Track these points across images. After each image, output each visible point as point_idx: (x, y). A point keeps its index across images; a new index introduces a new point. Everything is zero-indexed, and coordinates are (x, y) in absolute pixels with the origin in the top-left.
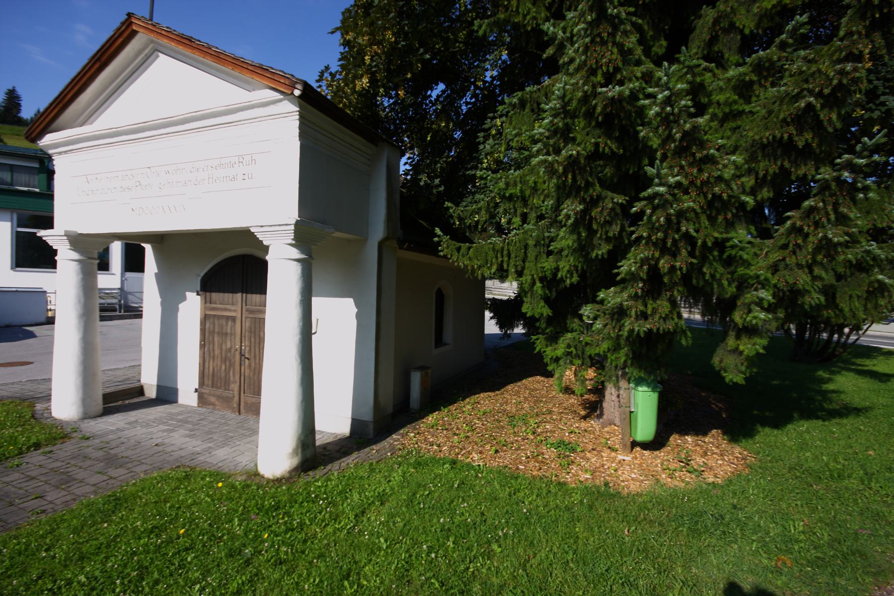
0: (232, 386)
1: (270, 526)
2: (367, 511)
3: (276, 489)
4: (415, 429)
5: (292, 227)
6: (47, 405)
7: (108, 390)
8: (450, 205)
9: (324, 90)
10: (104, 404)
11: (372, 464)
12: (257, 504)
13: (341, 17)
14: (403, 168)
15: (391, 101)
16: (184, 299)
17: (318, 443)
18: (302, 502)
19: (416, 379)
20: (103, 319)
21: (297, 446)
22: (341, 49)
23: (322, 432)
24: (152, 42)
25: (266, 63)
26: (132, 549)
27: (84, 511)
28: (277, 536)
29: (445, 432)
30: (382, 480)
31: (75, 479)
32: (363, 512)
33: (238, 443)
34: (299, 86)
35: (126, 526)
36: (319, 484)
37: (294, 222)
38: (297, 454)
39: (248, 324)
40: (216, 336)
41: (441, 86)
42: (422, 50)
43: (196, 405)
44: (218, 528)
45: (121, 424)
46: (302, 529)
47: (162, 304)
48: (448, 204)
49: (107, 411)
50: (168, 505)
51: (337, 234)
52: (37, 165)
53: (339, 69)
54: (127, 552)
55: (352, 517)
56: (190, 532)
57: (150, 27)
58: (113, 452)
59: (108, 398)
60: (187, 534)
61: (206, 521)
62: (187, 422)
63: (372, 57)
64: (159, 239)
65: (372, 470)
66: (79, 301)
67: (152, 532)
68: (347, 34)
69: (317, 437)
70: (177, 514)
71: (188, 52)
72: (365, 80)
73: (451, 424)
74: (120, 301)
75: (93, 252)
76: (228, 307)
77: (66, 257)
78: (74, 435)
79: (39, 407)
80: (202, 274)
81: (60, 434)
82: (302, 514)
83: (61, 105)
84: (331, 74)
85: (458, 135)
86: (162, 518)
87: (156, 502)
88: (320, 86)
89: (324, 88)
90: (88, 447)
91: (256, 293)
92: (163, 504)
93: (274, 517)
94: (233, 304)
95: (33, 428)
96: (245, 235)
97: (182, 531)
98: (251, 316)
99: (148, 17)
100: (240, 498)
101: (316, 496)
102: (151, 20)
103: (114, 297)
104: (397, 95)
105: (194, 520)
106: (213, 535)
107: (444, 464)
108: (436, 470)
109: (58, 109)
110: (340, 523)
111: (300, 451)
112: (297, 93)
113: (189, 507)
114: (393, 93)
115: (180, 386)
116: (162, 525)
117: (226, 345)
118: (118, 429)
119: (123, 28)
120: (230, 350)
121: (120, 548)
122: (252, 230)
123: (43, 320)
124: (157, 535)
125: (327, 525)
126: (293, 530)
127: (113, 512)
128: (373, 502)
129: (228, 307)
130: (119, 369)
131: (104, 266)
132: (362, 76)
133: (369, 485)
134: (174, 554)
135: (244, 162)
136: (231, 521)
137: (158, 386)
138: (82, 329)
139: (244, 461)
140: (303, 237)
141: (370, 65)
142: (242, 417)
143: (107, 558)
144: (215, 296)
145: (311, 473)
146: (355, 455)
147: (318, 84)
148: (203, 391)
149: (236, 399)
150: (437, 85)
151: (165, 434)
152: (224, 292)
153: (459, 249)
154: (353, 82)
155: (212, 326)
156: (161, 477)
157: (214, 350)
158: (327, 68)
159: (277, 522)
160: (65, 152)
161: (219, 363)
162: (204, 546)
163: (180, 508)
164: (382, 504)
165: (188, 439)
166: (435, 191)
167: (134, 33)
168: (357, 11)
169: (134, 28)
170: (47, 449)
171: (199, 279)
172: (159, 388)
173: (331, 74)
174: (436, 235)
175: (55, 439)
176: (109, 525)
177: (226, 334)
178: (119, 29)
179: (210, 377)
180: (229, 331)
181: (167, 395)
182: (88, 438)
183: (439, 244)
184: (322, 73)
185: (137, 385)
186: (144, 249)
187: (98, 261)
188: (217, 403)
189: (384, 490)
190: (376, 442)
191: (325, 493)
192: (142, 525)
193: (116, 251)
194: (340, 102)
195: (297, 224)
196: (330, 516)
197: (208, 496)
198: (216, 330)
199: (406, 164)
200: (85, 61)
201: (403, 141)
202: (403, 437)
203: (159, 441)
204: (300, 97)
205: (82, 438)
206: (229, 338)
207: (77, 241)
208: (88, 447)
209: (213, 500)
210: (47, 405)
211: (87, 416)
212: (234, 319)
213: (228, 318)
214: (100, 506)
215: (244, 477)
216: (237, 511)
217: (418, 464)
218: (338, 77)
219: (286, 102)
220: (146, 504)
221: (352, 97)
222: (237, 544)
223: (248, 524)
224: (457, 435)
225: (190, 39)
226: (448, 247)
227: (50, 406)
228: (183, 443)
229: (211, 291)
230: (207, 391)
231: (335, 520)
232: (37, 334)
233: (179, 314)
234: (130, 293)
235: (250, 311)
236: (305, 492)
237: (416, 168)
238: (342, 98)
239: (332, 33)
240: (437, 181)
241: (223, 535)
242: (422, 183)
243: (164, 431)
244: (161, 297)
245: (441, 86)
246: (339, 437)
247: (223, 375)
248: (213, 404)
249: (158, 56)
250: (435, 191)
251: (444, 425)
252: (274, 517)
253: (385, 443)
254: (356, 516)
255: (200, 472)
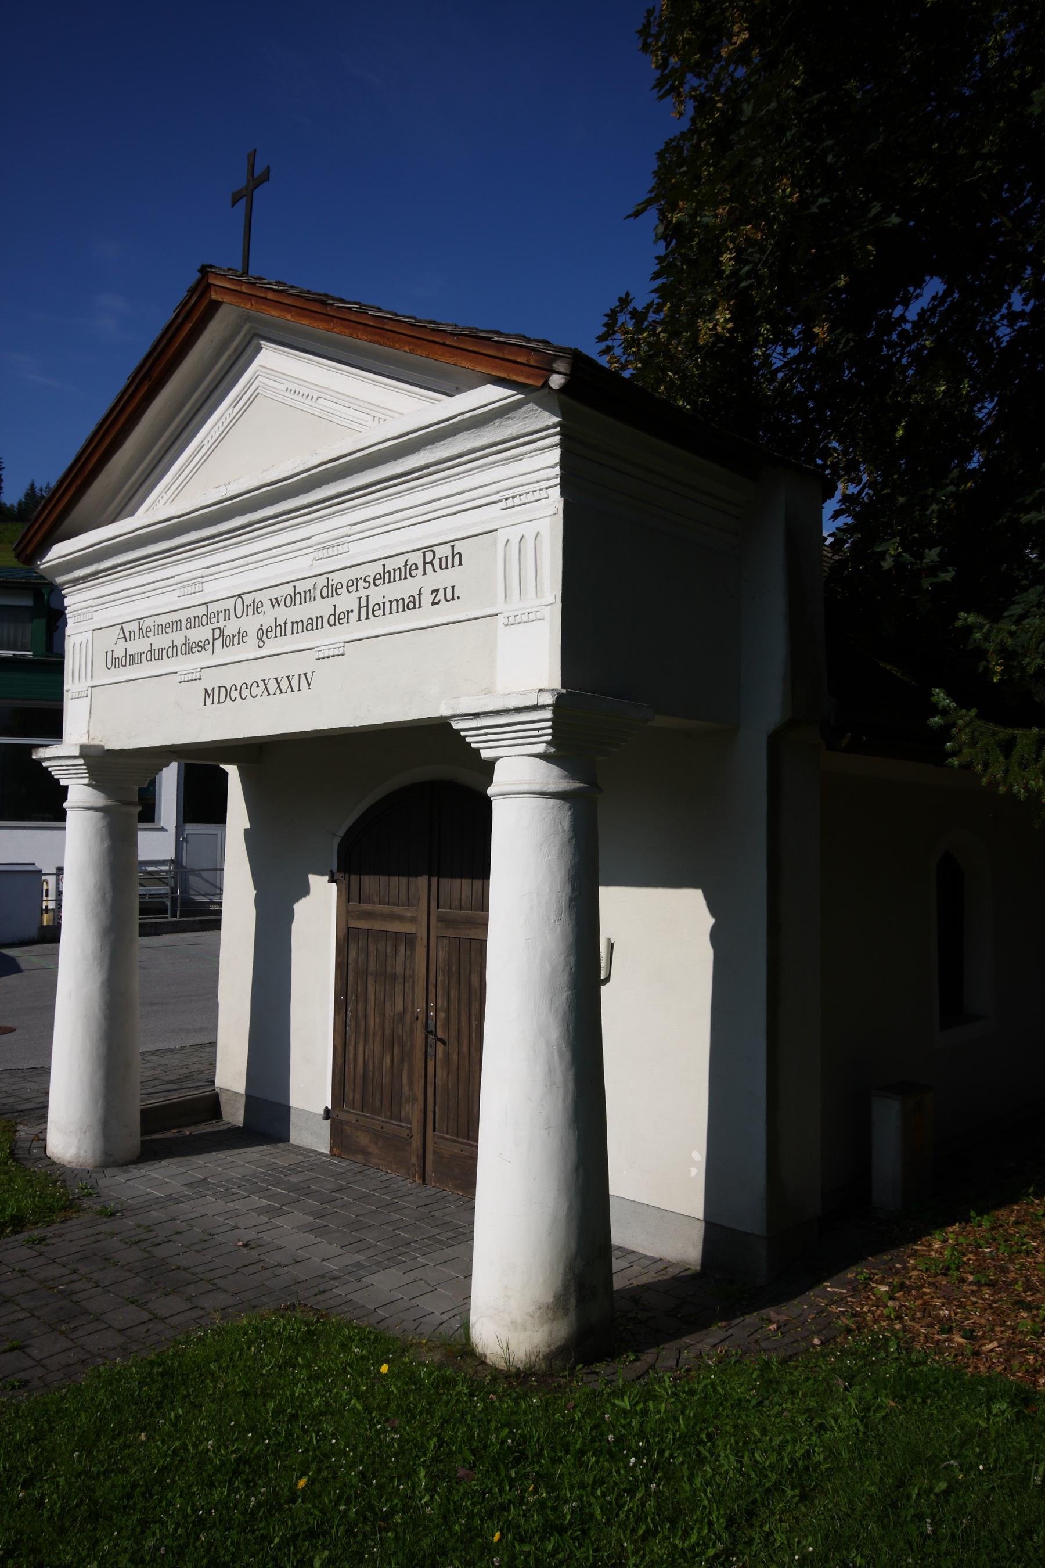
0: (407, 1108)
1: (504, 1508)
2: (763, 1513)
3: (516, 1401)
4: (893, 1272)
5: (548, 714)
6: (36, 1130)
7: (152, 1102)
8: (972, 619)
9: (616, 359)
10: (143, 1134)
11: (767, 1364)
12: (471, 1438)
13: (654, 164)
14: (828, 528)
15: (793, 352)
16: (304, 890)
17: (618, 1283)
18: (582, 1452)
19: (888, 1119)
20: (145, 931)
21: (566, 1287)
22: (661, 249)
23: (627, 1252)
24: (248, 319)
25: (484, 323)
26: (195, 1511)
27: (101, 1395)
28: (522, 1541)
29: (987, 1293)
30: (800, 1420)
31: (87, 1312)
32: (751, 1514)
33: (422, 1260)
34: (561, 366)
35: (184, 1446)
36: (626, 1404)
37: (548, 699)
38: (566, 1311)
39: (441, 954)
40: (371, 979)
41: (934, 286)
42: (876, 208)
43: (327, 1151)
44: (380, 1487)
45: (175, 1186)
46: (584, 1532)
47: (259, 902)
48: (966, 618)
49: (150, 1152)
50: (271, 1405)
51: (661, 721)
52: (29, 603)
53: (655, 298)
54: (186, 1517)
55: (720, 1524)
56: (317, 1487)
57: (244, 289)
58: (160, 1252)
59: (153, 1119)
60: (311, 1494)
61: (352, 1465)
62: (310, 1194)
63: (739, 251)
64: (253, 753)
65: (770, 1385)
66: (104, 897)
67: (236, 1473)
68: (673, 207)
69: (617, 1264)
70: (290, 1433)
71: (318, 328)
72: (722, 316)
73: (1004, 1270)
74: (173, 890)
75: (128, 778)
76: (398, 910)
77: (80, 793)
78: (86, 1203)
79: (24, 1132)
80: (342, 832)
81: (62, 1196)
82: (582, 1486)
83: (78, 482)
84: (634, 314)
85: (986, 409)
86: (258, 1439)
87: (245, 1394)
88: (608, 350)
89: (618, 352)
90: (112, 1235)
91: (462, 876)
92: (260, 1399)
93: (512, 1482)
94: (408, 904)
95: (11, 1180)
96: (436, 736)
97: (302, 1483)
98: (450, 933)
99: (239, 267)
100: (430, 1412)
101: (619, 1439)
102: (246, 272)
103: (162, 882)
104: (809, 336)
105: (327, 1456)
106: (370, 1507)
107: (991, 1398)
108: (965, 1416)
109: (73, 489)
110: (686, 1534)
111: (573, 1301)
112: (556, 381)
113: (315, 1418)
114: (797, 331)
115: (296, 1101)
116: (258, 1457)
117: (393, 1004)
118: (169, 1197)
119: (193, 301)
120: (402, 1016)
121: (171, 1503)
122: (456, 725)
123: (33, 932)
124: (246, 1482)
125: (650, 1534)
126: (561, 1530)
127: (159, 1405)
128: (777, 1486)
129: (398, 910)
130: (172, 1051)
131: (148, 814)
132: (714, 305)
133: (764, 1432)
134: (285, 1543)
135: (436, 562)
136: (409, 1474)
137: (248, 1096)
138: (107, 961)
139: (436, 1308)
140: (578, 730)
141: (735, 273)
142: (429, 1190)
143: (144, 1524)
144: (370, 883)
145: (601, 1367)
146: (717, 1331)
147: (602, 346)
148: (343, 1116)
149: (416, 1143)
150: (919, 283)
151: (264, 1218)
152: (389, 873)
153: (1007, 747)
154: (692, 325)
155: (362, 957)
156: (256, 1329)
157: (366, 1016)
158: (625, 301)
159: (522, 1501)
160: (85, 578)
161: (378, 1048)
162: (349, 1532)
163: (294, 1417)
164: (803, 1497)
165: (311, 1237)
166: (926, 584)
167: (214, 307)
168: (697, 146)
169: (214, 296)
170: (36, 1233)
171: (337, 841)
172: (251, 1100)
173: (634, 314)
174: (935, 710)
175: (51, 1210)
176: (149, 1438)
177: (394, 977)
178: (184, 305)
179: (359, 1081)
180: (399, 970)
181: (267, 1114)
182: (113, 1214)
183: (945, 733)
184: (613, 315)
185: (206, 1091)
186: (225, 774)
187: (140, 809)
188: (373, 1149)
189: (807, 1455)
190: (776, 1299)
191: (642, 1435)
192: (217, 1450)
193: (169, 780)
194: (659, 382)
195: (560, 705)
196: (659, 1508)
197: (357, 1394)
198: (372, 968)
199: (836, 515)
200: (122, 383)
201: (826, 452)
202: (855, 1292)
203: (252, 1234)
204: (563, 390)
205: (100, 1213)
206: (399, 987)
207: (101, 764)
208: (112, 1235)
209: (368, 1409)
210: (36, 1130)
211: (112, 1158)
212: (410, 940)
213: (396, 937)
214: (134, 1385)
215: (437, 1357)
216: (422, 1449)
217: (907, 1387)
218: (652, 317)
219: (531, 406)
220: (225, 1395)
221: (689, 364)
222: (425, 1542)
223: (450, 1489)
224: (1028, 1307)
225: (323, 300)
226: (973, 743)
227: (44, 1131)
228: (300, 1245)
229: (360, 873)
230: (352, 1118)
231: (673, 1522)
232: (23, 966)
233: (295, 926)
234: (193, 871)
235: (448, 922)
236: (589, 1424)
237: (867, 518)
238: (664, 370)
239: (637, 214)
240: (932, 555)
241: (393, 1511)
242: (887, 564)
243: (261, 1211)
244: (257, 885)
245: (934, 286)
246: (672, 1272)
247: (386, 1080)
248: (366, 1153)
249: (259, 349)
250: (926, 584)
251: (980, 1269)
252: (512, 1482)
253: (802, 1306)
254: (731, 1521)
255: (339, 1328)
